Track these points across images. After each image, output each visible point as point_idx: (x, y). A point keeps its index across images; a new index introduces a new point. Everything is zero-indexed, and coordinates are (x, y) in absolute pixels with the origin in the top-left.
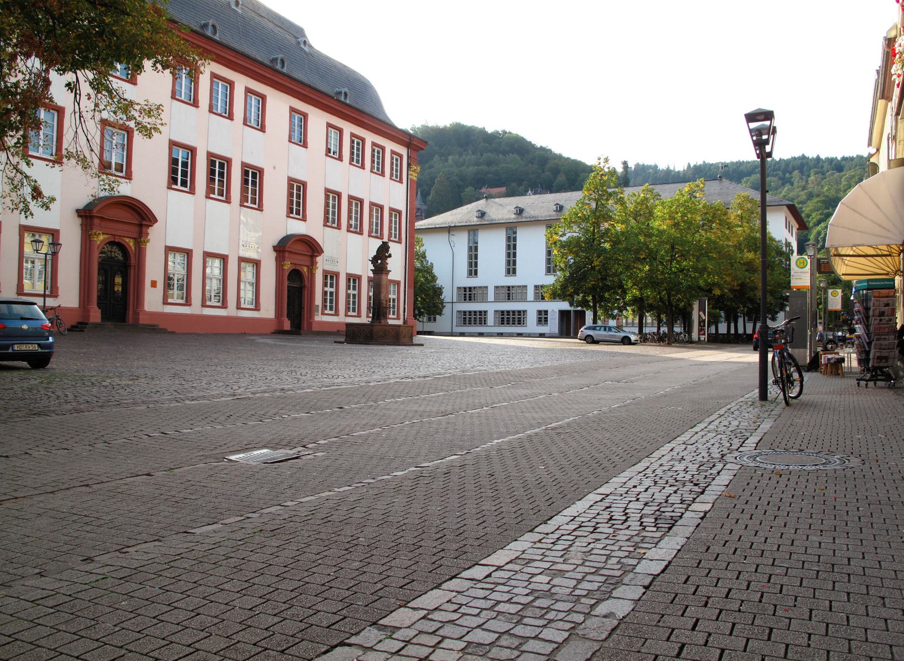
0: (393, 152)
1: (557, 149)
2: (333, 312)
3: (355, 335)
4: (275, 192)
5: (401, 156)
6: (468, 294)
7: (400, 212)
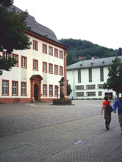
0: (60, 51)
1: (99, 45)
2: (25, 95)
3: (56, 102)
4: (30, 63)
5: (62, 52)
6: (78, 88)
7: (62, 67)
